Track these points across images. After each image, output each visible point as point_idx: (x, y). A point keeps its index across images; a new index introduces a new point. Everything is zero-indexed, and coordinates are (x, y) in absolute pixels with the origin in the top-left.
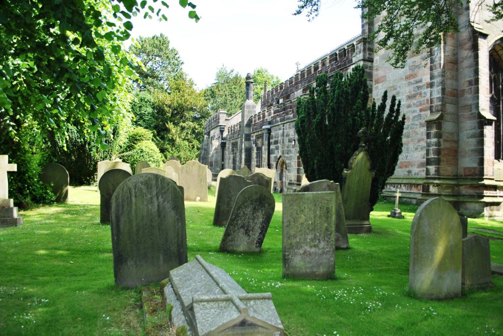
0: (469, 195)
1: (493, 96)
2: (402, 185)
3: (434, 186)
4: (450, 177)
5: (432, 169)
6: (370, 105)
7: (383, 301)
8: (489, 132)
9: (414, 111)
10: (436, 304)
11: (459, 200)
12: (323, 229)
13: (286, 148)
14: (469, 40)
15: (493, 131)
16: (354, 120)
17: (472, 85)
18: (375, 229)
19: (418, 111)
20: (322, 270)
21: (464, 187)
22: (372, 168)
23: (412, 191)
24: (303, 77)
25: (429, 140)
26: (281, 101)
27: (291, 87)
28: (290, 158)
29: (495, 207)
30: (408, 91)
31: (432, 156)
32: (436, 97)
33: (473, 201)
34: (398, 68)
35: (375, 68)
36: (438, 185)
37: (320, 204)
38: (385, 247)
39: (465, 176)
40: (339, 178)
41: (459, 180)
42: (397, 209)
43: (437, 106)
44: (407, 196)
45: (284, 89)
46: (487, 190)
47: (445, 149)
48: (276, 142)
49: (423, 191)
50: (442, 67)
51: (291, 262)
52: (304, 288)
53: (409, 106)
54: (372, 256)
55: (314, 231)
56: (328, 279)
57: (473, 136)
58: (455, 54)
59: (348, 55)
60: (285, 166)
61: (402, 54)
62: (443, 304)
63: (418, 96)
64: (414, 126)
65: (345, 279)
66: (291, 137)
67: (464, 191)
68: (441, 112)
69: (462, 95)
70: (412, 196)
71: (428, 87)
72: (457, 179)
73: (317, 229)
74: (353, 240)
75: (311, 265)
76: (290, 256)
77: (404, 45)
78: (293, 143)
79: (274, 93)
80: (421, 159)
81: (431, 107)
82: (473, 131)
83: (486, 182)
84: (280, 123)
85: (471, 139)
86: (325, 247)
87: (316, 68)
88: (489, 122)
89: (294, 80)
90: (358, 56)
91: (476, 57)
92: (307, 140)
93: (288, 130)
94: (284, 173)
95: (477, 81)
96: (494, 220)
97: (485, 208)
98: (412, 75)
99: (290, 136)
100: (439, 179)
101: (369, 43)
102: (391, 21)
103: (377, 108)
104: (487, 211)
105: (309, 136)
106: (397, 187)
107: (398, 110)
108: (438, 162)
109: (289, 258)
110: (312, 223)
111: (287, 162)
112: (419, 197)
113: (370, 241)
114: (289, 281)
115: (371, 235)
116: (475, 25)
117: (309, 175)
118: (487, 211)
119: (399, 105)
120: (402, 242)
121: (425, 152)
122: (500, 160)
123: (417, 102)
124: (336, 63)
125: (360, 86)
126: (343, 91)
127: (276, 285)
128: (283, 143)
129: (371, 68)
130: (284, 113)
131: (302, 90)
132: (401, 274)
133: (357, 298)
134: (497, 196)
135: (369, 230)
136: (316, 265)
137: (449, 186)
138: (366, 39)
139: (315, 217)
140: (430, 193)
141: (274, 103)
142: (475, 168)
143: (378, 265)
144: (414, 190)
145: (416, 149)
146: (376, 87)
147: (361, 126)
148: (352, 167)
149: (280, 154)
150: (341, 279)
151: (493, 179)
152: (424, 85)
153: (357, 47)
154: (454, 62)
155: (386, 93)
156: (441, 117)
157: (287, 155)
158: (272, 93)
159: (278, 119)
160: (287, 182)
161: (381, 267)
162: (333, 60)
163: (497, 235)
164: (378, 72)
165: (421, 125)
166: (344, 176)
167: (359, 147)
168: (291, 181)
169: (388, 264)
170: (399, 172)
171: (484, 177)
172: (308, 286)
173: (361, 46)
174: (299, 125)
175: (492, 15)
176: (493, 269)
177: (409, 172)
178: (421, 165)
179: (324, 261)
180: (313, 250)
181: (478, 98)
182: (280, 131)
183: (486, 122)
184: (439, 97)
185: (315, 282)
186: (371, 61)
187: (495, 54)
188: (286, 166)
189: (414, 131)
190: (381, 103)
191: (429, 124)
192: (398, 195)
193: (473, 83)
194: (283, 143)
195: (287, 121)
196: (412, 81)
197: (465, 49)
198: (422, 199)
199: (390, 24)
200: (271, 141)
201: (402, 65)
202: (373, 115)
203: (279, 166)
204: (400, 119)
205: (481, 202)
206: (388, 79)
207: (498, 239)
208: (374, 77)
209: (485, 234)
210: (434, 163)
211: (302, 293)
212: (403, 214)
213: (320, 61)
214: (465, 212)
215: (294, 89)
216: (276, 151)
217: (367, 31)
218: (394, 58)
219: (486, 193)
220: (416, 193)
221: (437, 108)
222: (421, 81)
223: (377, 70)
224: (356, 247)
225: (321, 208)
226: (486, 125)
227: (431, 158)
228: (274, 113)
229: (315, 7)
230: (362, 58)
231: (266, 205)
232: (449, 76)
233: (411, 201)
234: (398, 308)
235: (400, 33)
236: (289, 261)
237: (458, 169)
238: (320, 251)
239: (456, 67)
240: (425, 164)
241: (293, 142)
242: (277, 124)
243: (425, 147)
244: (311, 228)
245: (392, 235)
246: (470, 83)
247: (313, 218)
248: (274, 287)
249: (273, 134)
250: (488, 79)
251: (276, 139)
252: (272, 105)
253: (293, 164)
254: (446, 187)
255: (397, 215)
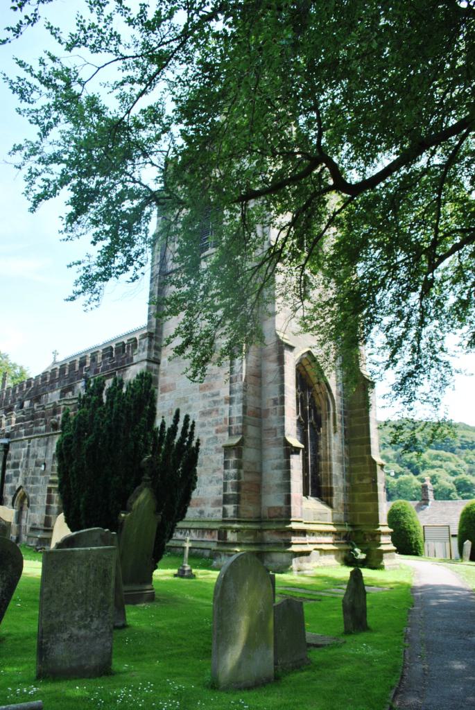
0: (275, 543)
1: (299, 418)
2: (192, 531)
3: (232, 532)
4: (252, 520)
5: (231, 508)
6: (158, 423)
7: (181, 698)
8: (296, 462)
9: (209, 432)
10: (246, 694)
11: (263, 550)
12: (98, 601)
13: (30, 476)
14: (274, 352)
15: (301, 461)
16: (136, 445)
17: (277, 405)
18: (159, 596)
19: (214, 432)
20: (94, 662)
21: (268, 532)
22: (157, 511)
23: (204, 539)
24: (64, 375)
25: (226, 471)
26: (27, 404)
27: (43, 385)
28: (36, 491)
29: (304, 558)
30: (202, 405)
31: (230, 492)
32: (236, 416)
33: (279, 550)
34: (196, 382)
35: (162, 372)
36: (237, 530)
37: (95, 565)
38: (175, 621)
39: (270, 518)
40: (115, 525)
41: (262, 523)
42: (186, 565)
43: (237, 427)
44: (198, 545)
45: (32, 386)
46: (295, 536)
47: (248, 482)
48: (16, 465)
49: (219, 539)
50: (243, 380)
51: (49, 653)
52: (71, 691)
53: (203, 425)
54: (158, 636)
55: (86, 604)
56: (101, 676)
57: (278, 467)
58: (259, 366)
59: (128, 352)
60: (26, 502)
61: (201, 363)
62: (254, 693)
63: (214, 413)
64: (208, 452)
65: (125, 672)
66: (40, 458)
67: (269, 537)
68: (241, 436)
69: (266, 416)
70: (204, 545)
71: (226, 403)
72: (261, 522)
73: (90, 601)
74: (133, 615)
75: (78, 656)
76: (49, 644)
77: (203, 355)
78: (43, 468)
79: (17, 392)
80: (216, 496)
81: (230, 429)
82: (279, 461)
83: (294, 526)
84: (24, 437)
85: (275, 471)
86: (100, 626)
87: (83, 363)
88: (296, 451)
89: (49, 376)
90: (141, 354)
91: (282, 371)
92: (73, 468)
93: (36, 448)
94: (25, 513)
95: (282, 400)
96: (303, 575)
97: (294, 560)
98: (207, 386)
99: (38, 458)
100: (239, 522)
101: (157, 339)
102: (191, 325)
103: (166, 429)
104: (295, 563)
105: (76, 463)
106: (185, 534)
107: (192, 434)
108: (237, 500)
109: (47, 648)
110: (83, 593)
111: (31, 495)
112: (214, 546)
113: (154, 614)
114: (47, 682)
115: (155, 606)
116: (281, 335)
117: (71, 520)
118: (295, 563)
119: (193, 426)
120: (196, 612)
121: (222, 486)
122: (309, 497)
123: (213, 420)
124: (110, 359)
125: (146, 399)
126: (124, 405)
127: (28, 691)
128: (27, 466)
129: (157, 371)
130: (31, 423)
131: (59, 391)
132: (198, 658)
133: (146, 698)
134: (306, 544)
135: (152, 598)
136: (85, 655)
137: (250, 532)
138: (152, 334)
139: (87, 584)
140: (227, 541)
141: (16, 406)
142: (280, 508)
143: (168, 648)
144: (207, 537)
145: (211, 482)
146: (161, 397)
147: (146, 451)
148: (131, 509)
149: (20, 483)
150: (120, 673)
151: (301, 522)
152: (222, 400)
153: (140, 343)
154: (257, 376)
155: (178, 412)
156: (241, 442)
157: (31, 486)
158: (14, 391)
159: (23, 431)
160: (29, 526)
161: (171, 650)
162: (107, 355)
163: (309, 594)
164: (166, 378)
165: (218, 451)
166: (121, 521)
167: (141, 481)
168: (35, 524)
169: (180, 645)
170: (191, 513)
171: (292, 519)
172: (77, 688)
173: (145, 342)
174: (63, 446)
175: (299, 328)
176: (308, 641)
177: (201, 512)
178: (217, 503)
179: (97, 647)
180: (83, 632)
181: (283, 420)
182: (23, 449)
183: (293, 450)
184: (240, 417)
185: (86, 681)
186: (158, 362)
187: (301, 369)
188: (28, 502)
189: (209, 458)
190: (172, 426)
191: (227, 450)
192: (188, 545)
193: (278, 402)
194: (27, 466)
195: (35, 435)
196: (207, 393)
197: (270, 362)
198: (217, 550)
199: (189, 328)
200: (7, 463)
201: (201, 379)
202: (162, 437)
203: (17, 502)
204: (194, 444)
205: (289, 552)
206: (177, 388)
207: (311, 600)
208: (160, 383)
209: (295, 595)
210: (233, 501)
211: (69, 699)
212: (194, 571)
213: (89, 355)
214: (271, 566)
215: (47, 389)
216: (14, 479)
217: (154, 324)
218: (192, 369)
219: (294, 539)
220: (210, 541)
221: (237, 430)
222: (218, 394)
223: (164, 375)
224: (136, 624)
225: (96, 570)
226: (292, 453)
227: (230, 494)
228: (17, 422)
229: (96, 296)
230: (146, 357)
231: (10, 566)
232: (252, 392)
233: (203, 554)
234: (201, 705)
235: (200, 340)
236: (47, 652)
237: (261, 508)
238: (92, 634)
239: (259, 381)
240: (222, 502)
241: (43, 466)
242: (19, 438)
243: (221, 480)
244: (81, 600)
245: (183, 603)
246: (275, 402)
247: (84, 586)
248: (27, 693)
249: (12, 452)
250: (295, 398)
251: (16, 461)
252: (11, 409)
253: (39, 499)
254: (247, 532)
255: (186, 574)
